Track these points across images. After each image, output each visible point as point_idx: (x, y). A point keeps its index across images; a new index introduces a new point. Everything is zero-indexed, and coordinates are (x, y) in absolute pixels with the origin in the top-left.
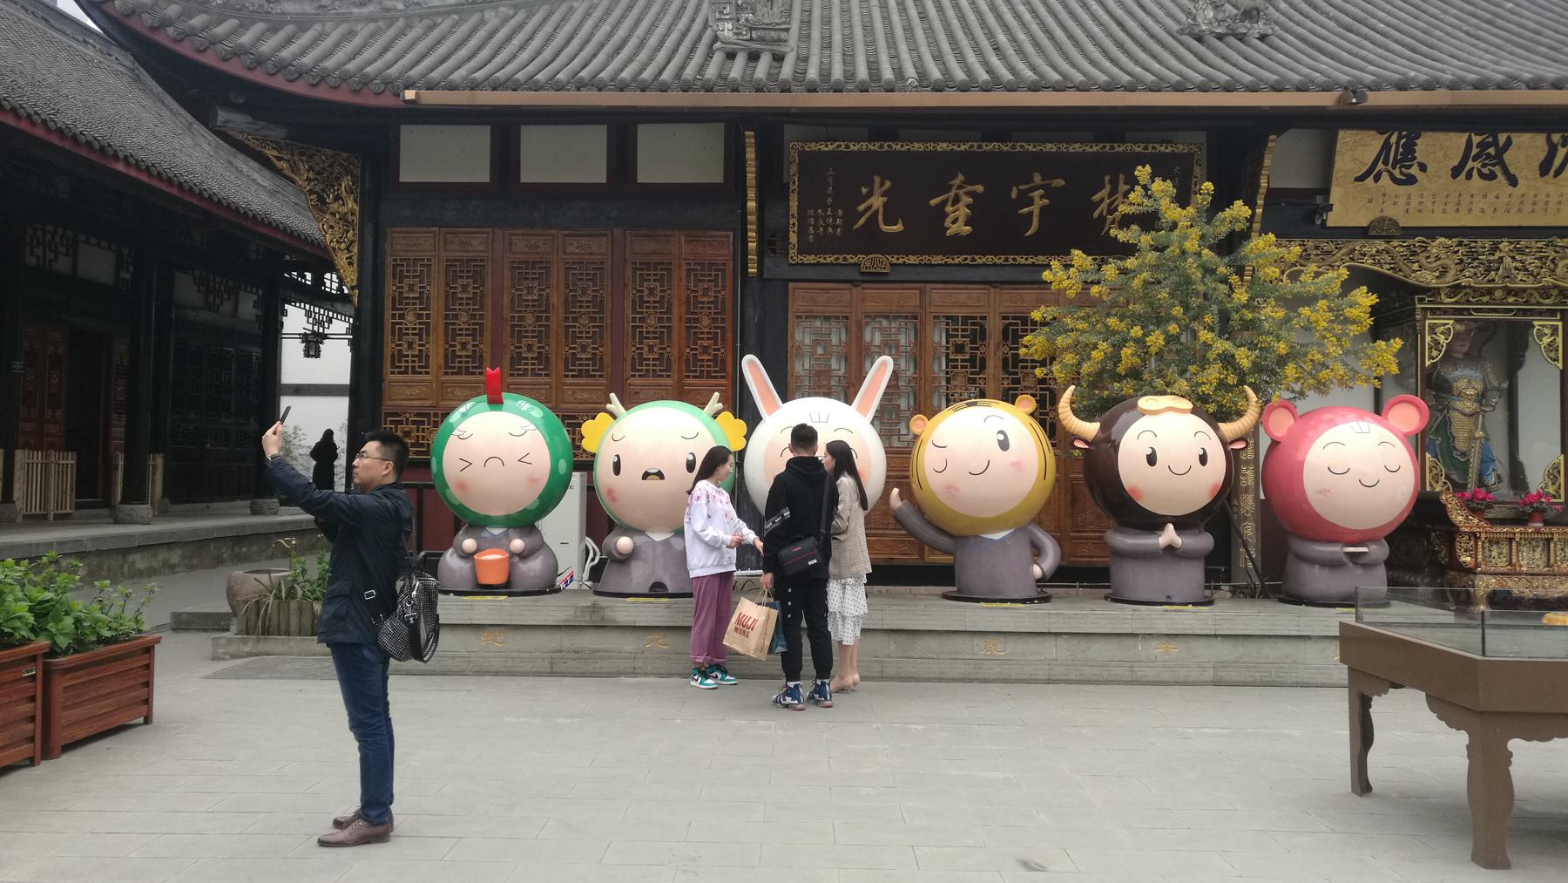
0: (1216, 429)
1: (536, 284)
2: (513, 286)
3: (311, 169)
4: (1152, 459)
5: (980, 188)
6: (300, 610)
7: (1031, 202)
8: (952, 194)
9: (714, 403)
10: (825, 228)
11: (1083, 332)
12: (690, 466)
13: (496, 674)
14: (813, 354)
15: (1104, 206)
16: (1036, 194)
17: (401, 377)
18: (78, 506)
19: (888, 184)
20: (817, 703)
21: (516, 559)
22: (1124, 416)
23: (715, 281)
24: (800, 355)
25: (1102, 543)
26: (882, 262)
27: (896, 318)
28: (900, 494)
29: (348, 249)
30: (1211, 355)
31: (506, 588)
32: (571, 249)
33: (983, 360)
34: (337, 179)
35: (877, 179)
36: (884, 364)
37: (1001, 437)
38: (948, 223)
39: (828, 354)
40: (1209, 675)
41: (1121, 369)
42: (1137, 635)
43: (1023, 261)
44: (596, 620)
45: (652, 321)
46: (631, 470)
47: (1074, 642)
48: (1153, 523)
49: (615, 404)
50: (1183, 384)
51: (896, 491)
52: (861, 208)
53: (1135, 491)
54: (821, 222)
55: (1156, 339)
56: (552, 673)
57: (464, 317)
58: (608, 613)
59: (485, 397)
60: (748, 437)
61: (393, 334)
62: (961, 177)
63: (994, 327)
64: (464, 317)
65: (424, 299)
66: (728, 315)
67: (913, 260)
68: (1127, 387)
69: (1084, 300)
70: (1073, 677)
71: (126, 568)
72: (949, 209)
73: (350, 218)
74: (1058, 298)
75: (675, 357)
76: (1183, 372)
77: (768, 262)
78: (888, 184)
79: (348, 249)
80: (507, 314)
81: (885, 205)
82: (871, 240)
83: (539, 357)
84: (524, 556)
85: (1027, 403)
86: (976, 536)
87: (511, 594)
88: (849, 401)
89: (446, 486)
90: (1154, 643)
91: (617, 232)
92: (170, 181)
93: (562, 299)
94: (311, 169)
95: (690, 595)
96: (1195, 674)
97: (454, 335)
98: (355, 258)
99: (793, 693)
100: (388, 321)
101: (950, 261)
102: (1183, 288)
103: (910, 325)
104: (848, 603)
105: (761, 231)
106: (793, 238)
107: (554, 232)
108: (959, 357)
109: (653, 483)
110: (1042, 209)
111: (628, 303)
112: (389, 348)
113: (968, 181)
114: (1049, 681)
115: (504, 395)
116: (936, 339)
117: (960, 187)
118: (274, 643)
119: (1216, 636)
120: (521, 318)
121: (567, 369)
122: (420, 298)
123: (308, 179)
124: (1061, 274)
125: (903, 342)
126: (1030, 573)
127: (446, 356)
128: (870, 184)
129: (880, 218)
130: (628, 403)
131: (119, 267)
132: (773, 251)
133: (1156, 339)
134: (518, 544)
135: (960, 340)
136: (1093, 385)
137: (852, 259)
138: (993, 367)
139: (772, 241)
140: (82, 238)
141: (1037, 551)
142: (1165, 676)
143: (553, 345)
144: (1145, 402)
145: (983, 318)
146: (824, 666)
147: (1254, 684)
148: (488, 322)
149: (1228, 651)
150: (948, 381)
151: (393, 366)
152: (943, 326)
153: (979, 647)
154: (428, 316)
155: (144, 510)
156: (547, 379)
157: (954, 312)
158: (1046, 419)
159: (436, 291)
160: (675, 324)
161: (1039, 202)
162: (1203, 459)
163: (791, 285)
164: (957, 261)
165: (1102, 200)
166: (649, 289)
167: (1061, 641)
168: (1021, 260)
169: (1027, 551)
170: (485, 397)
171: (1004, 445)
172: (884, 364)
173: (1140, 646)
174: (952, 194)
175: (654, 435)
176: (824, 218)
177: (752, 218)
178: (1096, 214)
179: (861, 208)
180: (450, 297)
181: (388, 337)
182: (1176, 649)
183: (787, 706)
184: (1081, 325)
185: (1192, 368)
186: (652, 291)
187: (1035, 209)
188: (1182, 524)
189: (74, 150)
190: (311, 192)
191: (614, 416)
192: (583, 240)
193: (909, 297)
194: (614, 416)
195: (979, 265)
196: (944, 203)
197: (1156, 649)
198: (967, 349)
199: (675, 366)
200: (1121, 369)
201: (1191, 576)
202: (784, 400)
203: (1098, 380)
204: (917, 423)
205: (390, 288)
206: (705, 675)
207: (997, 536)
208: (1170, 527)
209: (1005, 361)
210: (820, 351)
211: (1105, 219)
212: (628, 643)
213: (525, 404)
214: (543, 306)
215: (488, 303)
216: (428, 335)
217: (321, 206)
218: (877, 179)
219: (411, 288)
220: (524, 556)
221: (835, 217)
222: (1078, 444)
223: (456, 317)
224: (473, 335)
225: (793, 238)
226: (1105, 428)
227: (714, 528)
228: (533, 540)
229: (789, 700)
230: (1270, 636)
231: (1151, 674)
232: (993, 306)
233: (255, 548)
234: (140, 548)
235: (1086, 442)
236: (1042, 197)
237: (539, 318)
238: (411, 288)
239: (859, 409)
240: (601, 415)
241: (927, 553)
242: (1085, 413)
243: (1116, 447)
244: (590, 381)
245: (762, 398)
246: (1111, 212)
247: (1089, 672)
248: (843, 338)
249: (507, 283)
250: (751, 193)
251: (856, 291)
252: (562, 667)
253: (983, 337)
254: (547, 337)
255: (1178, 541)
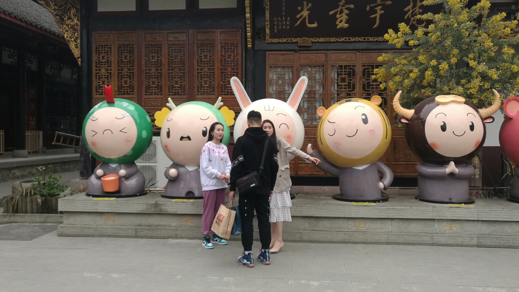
0: (478, 112)
1: (156, 54)
2: (146, 56)
3: (55, 5)
4: (444, 128)
5: (352, 6)
6: (32, 201)
7: (375, 12)
8: (339, 9)
9: (219, 102)
10: (282, 26)
11: (404, 65)
12: (204, 133)
13: (110, 236)
14: (277, 84)
15: (410, 13)
16: (378, 8)
17: (99, 96)
18: (6, 150)
19: (310, 5)
20: (262, 261)
21: (123, 179)
22: (427, 107)
23: (233, 51)
24: (271, 84)
25: (416, 171)
26: (308, 41)
27: (314, 67)
28: (312, 146)
29: (75, 41)
30: (475, 74)
31: (117, 194)
32: (170, 39)
33: (354, 85)
34: (69, 10)
35: (305, 3)
36: (303, 80)
37: (364, 117)
38: (338, 22)
39: (284, 84)
40: (475, 242)
41: (425, 83)
42: (434, 220)
43: (372, 40)
44: (157, 211)
45: (206, 70)
46: (175, 136)
47: (401, 223)
48: (443, 161)
49: (171, 103)
50: (460, 89)
51: (310, 145)
52: (298, 16)
53: (434, 144)
54: (280, 23)
55: (444, 66)
56: (136, 237)
57: (126, 70)
58: (163, 208)
59: (105, 101)
60: (235, 119)
61: (96, 78)
62: (343, 1)
63: (359, 70)
64: (126, 70)
65: (109, 63)
66: (240, 67)
67: (322, 40)
68: (428, 92)
69: (406, 47)
70: (400, 241)
71: (11, 175)
72: (338, 16)
73: (76, 27)
74: (393, 49)
75: (216, 86)
76: (458, 84)
77: (256, 42)
78: (310, 5)
79: (75, 41)
80: (144, 68)
81: (309, 15)
82: (302, 31)
83: (157, 87)
84: (127, 177)
85: (377, 100)
86: (351, 168)
87: (118, 197)
88: (285, 100)
89: (88, 144)
90: (444, 224)
91: (191, 31)
92: (21, 20)
93: (167, 61)
94: (55, 5)
95: (201, 198)
96: (467, 241)
97: (122, 78)
98: (79, 45)
99: (247, 257)
100: (94, 72)
101: (339, 40)
102: (458, 39)
103: (321, 70)
104: (281, 205)
105: (253, 27)
106: (268, 31)
107: (163, 31)
108: (343, 84)
109: (185, 142)
110: (381, 15)
111: (195, 62)
112: (95, 84)
113: (347, 3)
114: (388, 243)
115: (114, 99)
116: (333, 76)
117: (343, 6)
118: (19, 217)
119: (478, 221)
120: (150, 70)
121: (169, 92)
122: (107, 62)
123: (54, 9)
124: (394, 35)
125: (317, 77)
126: (377, 186)
127: (118, 87)
128: (302, 5)
129: (307, 21)
130: (178, 103)
131: (72, 74)
132: (259, 37)
133: (444, 66)
134: (123, 172)
135: (343, 76)
136: (409, 92)
137: (294, 40)
138: (358, 88)
139: (258, 33)
140: (65, 66)
141: (382, 176)
142: (450, 242)
143: (163, 81)
144: (439, 99)
145: (354, 66)
146: (266, 243)
147: (500, 247)
148: (135, 72)
149: (485, 229)
150: (338, 95)
151: (97, 91)
152: (336, 70)
153: (351, 226)
154: (111, 70)
155: (25, 152)
156: (161, 96)
157: (341, 63)
158: (386, 106)
159: (114, 59)
160: (216, 71)
161: (379, 12)
162: (472, 128)
163: (267, 53)
164: (342, 40)
165: (409, 10)
166: (205, 56)
167: (395, 223)
168: (371, 39)
169: (376, 176)
170: (105, 101)
171: (365, 121)
172: (303, 80)
173: (436, 225)
174: (339, 9)
175: (189, 116)
176: (282, 21)
177: (248, 22)
178: (406, 17)
179: (298, 16)
180: (120, 62)
181: (94, 79)
182: (456, 227)
183: (245, 264)
184: (403, 62)
185: (463, 81)
186: (205, 56)
187: (378, 15)
188: (458, 161)
189: (21, 24)
190: (56, 15)
191: (170, 109)
192: (176, 35)
193: (321, 57)
194: (170, 109)
195: (352, 42)
196: (336, 13)
197: (445, 227)
198: (347, 80)
199: (216, 90)
200: (425, 83)
201: (461, 189)
202: (252, 101)
203: (411, 89)
204: (320, 111)
205: (94, 58)
206: (208, 241)
207: (361, 168)
208: (452, 163)
209: (364, 86)
210: (280, 82)
211: (410, 19)
212: (174, 222)
213: (125, 103)
214: (159, 64)
215: (136, 63)
216: (111, 78)
217: (61, 21)
218: (305, 3)
219: (103, 57)
220: (127, 177)
221: (286, 21)
222: (403, 121)
223: (122, 70)
224: (130, 77)
225: (268, 31)
226: (417, 112)
227: (216, 165)
228: (132, 170)
229: (245, 261)
230: (508, 221)
231: (443, 240)
232: (358, 61)
233: (71, 166)
234: (17, 167)
235: (407, 119)
236: (381, 10)
237: (157, 70)
238: (103, 57)
239: (290, 104)
240: (164, 109)
241: (324, 174)
242: (406, 105)
243: (423, 123)
244: (180, 97)
245: (241, 99)
246: (413, 16)
247: (412, 239)
248: (291, 76)
249: (143, 54)
250: (248, 10)
251: (297, 55)
252: (141, 233)
253: (354, 75)
254: (161, 78)
255: (457, 170)
